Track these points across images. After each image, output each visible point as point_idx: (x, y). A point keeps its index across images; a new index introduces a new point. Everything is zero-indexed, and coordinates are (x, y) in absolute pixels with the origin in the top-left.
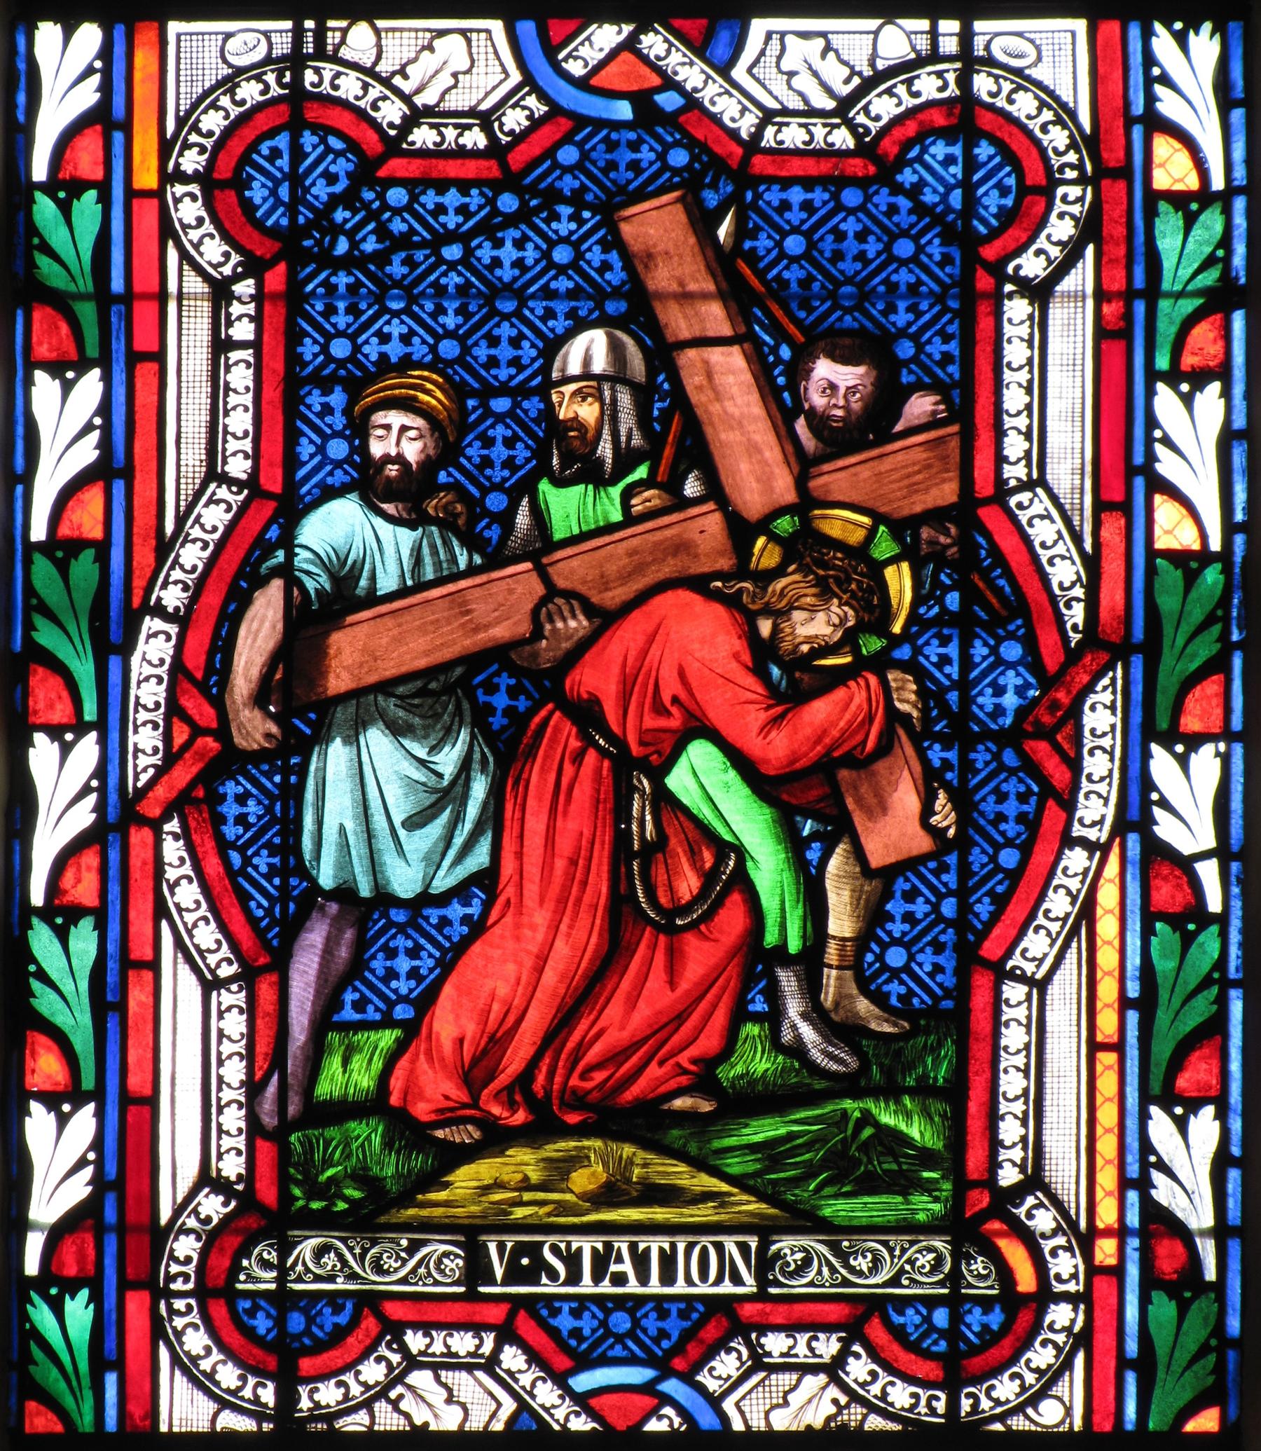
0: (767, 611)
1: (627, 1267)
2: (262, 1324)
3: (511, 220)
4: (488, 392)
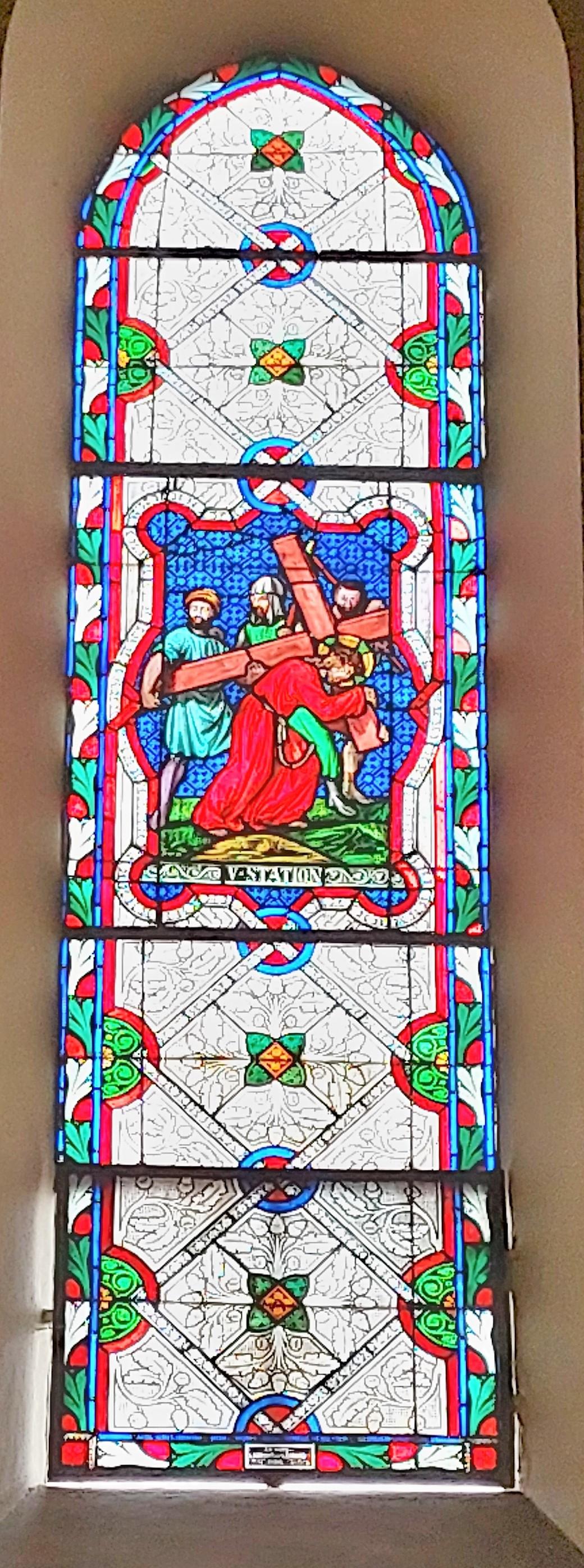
0: (324, 668)
1: (277, 876)
2: (151, 892)
3: (238, 543)
4: (230, 597)
